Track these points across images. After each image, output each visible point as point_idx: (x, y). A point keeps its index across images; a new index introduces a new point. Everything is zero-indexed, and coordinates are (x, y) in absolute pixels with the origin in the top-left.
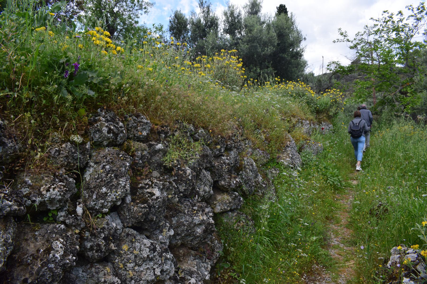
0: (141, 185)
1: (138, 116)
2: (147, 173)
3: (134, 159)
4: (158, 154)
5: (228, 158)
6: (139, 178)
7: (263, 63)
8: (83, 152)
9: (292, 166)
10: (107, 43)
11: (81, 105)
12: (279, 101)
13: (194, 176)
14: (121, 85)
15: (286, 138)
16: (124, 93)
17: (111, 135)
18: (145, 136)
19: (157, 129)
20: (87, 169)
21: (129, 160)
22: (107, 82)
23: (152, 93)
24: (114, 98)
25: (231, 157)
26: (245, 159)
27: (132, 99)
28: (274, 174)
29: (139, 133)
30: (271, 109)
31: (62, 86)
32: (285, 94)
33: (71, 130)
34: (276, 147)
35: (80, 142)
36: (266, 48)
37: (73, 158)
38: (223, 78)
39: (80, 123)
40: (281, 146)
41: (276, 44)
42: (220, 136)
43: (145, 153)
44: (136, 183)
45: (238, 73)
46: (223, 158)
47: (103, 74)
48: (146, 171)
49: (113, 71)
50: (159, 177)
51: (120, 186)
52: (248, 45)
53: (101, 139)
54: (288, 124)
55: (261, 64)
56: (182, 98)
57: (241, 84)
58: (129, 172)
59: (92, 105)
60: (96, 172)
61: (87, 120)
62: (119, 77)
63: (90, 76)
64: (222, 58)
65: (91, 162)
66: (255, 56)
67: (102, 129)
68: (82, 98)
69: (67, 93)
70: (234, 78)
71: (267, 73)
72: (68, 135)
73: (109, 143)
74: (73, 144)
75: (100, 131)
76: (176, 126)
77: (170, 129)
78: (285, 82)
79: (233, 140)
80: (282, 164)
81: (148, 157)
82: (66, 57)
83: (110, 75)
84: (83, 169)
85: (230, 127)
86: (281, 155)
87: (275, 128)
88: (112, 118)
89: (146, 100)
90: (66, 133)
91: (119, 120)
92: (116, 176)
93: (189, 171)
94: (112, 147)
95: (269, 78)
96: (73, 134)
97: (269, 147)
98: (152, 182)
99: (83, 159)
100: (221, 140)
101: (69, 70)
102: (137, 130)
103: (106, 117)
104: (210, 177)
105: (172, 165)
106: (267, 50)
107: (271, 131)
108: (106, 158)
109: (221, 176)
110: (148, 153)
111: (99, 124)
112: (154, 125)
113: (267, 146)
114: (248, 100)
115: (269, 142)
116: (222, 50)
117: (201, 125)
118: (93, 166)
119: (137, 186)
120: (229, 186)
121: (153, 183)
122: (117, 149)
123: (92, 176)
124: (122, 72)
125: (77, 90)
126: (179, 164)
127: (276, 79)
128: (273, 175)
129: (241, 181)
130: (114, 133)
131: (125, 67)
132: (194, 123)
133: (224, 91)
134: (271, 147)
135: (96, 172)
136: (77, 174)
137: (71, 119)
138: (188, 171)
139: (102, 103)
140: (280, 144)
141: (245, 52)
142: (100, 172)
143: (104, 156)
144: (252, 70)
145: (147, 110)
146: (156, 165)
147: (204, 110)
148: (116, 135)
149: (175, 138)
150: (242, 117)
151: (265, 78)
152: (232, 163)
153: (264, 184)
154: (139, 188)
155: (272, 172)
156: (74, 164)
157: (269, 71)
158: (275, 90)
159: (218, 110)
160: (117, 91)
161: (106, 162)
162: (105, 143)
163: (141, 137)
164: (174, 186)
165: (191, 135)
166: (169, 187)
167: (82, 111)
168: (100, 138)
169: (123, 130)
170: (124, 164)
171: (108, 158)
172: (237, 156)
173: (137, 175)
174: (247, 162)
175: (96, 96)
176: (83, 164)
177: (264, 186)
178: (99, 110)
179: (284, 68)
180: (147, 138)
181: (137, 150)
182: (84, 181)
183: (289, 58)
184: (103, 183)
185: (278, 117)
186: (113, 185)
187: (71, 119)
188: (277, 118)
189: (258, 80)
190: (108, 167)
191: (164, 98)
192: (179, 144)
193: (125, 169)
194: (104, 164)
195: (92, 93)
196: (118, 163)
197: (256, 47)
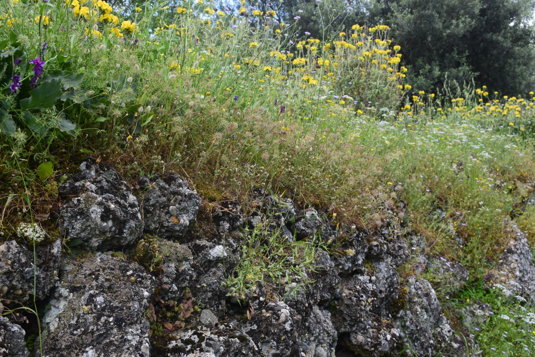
0: (174, 343)
1: (170, 180)
2: (188, 315)
3: (160, 280)
4: (213, 270)
5: (373, 278)
6: (169, 326)
7: (447, 55)
8: (44, 263)
9: (523, 299)
10: (103, 12)
11: (45, 153)
12: (487, 144)
13: (297, 322)
14: (132, 108)
15: (506, 232)
16: (139, 126)
17: (110, 223)
18: (185, 227)
19: (214, 211)
20: (53, 302)
21: (149, 283)
22: (103, 102)
23: (204, 127)
24: (117, 138)
25: (381, 275)
26: (412, 280)
27: (159, 141)
28: (477, 316)
29: (173, 220)
30: (471, 162)
31: (4, 111)
32: (501, 126)
33: (21, 210)
34: (482, 253)
35: (39, 240)
36: (454, 22)
37: (23, 277)
38: (358, 92)
39: (41, 195)
40: (494, 251)
41: (477, 11)
42: (354, 227)
43: (185, 266)
44: (163, 337)
45: (390, 79)
46: (361, 278)
47: (93, 84)
48: (187, 310)
49: (115, 77)
50: (216, 325)
51: (127, 346)
52: (412, 13)
53: (87, 232)
54: (510, 199)
55: (442, 57)
56: (268, 136)
57: (398, 103)
58: (149, 313)
59: (67, 154)
60: (74, 310)
61: (55, 187)
62: (130, 90)
63: (67, 86)
64: (353, 44)
65: (63, 286)
66: (429, 39)
67: (88, 209)
68: (47, 138)
69: (15, 127)
70: (382, 91)
71: (457, 78)
72: (12, 222)
73: (104, 242)
74: (24, 244)
75: (84, 214)
76: (255, 203)
77: (242, 210)
78: (500, 97)
79: (383, 235)
80: (498, 294)
81: (191, 276)
82: (16, 45)
83: (108, 85)
84: (43, 304)
85: (376, 206)
86: (495, 272)
87: (480, 206)
88: (113, 185)
89: (188, 142)
90: (9, 218)
91: (128, 189)
92: (119, 322)
93: (285, 312)
94: (111, 252)
95: (462, 89)
96: (24, 221)
97: (465, 252)
98: (200, 335)
99: (44, 279)
100: (358, 236)
101: (22, 74)
102: (168, 213)
103: (100, 182)
104: (331, 324)
105: (246, 295)
106: (457, 26)
107: (469, 214)
108: (97, 279)
109: (356, 321)
110: (193, 266)
111: (82, 197)
112: (206, 202)
113: (462, 249)
114: (415, 141)
115: (466, 240)
116: (354, 27)
117: (312, 199)
118: (66, 297)
119: (166, 345)
120: (375, 346)
121: (202, 339)
122: (121, 256)
123: (64, 321)
124: (137, 79)
125: (38, 120)
126: (263, 294)
127: (479, 91)
128: (476, 320)
129: (402, 334)
130: (115, 219)
131: (142, 65)
132: (300, 200)
133: (363, 120)
134: (471, 251)
135: (74, 310)
136: (31, 316)
137: (21, 186)
138: (283, 310)
139: (89, 148)
140: (491, 245)
141: (406, 29)
142: (81, 312)
143: (93, 273)
144: (421, 72)
145: (189, 166)
146: (210, 294)
147: (318, 164)
148: (120, 224)
149: (256, 232)
150: (403, 180)
151: (453, 90)
152: (381, 292)
153: (456, 341)
154: (169, 351)
155: (473, 314)
156: (25, 292)
157: (461, 74)
158: (477, 117)
159: (350, 165)
160: (123, 120)
161: (98, 287)
162: (95, 242)
163: (177, 228)
164: (252, 348)
165: (289, 225)
166: (240, 351)
167: (47, 169)
168: (83, 230)
169: (137, 212)
170: (137, 294)
171: (101, 279)
172: (394, 275)
173: (164, 318)
174: (416, 289)
175: (78, 133)
176: (44, 292)
177: (456, 345)
178: (83, 166)
179: (497, 65)
180: (189, 232)
181: (167, 259)
182: (45, 332)
183: (508, 44)
184: (88, 339)
185: (486, 182)
186: (111, 342)
187: (21, 186)
188: (482, 185)
189: (436, 94)
190: (100, 299)
191: (228, 136)
192: (262, 245)
193: (141, 305)
194: (92, 292)
195: (69, 127)
196: (125, 291)
197: (430, 19)
